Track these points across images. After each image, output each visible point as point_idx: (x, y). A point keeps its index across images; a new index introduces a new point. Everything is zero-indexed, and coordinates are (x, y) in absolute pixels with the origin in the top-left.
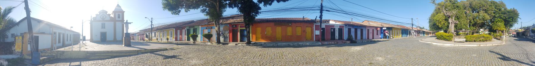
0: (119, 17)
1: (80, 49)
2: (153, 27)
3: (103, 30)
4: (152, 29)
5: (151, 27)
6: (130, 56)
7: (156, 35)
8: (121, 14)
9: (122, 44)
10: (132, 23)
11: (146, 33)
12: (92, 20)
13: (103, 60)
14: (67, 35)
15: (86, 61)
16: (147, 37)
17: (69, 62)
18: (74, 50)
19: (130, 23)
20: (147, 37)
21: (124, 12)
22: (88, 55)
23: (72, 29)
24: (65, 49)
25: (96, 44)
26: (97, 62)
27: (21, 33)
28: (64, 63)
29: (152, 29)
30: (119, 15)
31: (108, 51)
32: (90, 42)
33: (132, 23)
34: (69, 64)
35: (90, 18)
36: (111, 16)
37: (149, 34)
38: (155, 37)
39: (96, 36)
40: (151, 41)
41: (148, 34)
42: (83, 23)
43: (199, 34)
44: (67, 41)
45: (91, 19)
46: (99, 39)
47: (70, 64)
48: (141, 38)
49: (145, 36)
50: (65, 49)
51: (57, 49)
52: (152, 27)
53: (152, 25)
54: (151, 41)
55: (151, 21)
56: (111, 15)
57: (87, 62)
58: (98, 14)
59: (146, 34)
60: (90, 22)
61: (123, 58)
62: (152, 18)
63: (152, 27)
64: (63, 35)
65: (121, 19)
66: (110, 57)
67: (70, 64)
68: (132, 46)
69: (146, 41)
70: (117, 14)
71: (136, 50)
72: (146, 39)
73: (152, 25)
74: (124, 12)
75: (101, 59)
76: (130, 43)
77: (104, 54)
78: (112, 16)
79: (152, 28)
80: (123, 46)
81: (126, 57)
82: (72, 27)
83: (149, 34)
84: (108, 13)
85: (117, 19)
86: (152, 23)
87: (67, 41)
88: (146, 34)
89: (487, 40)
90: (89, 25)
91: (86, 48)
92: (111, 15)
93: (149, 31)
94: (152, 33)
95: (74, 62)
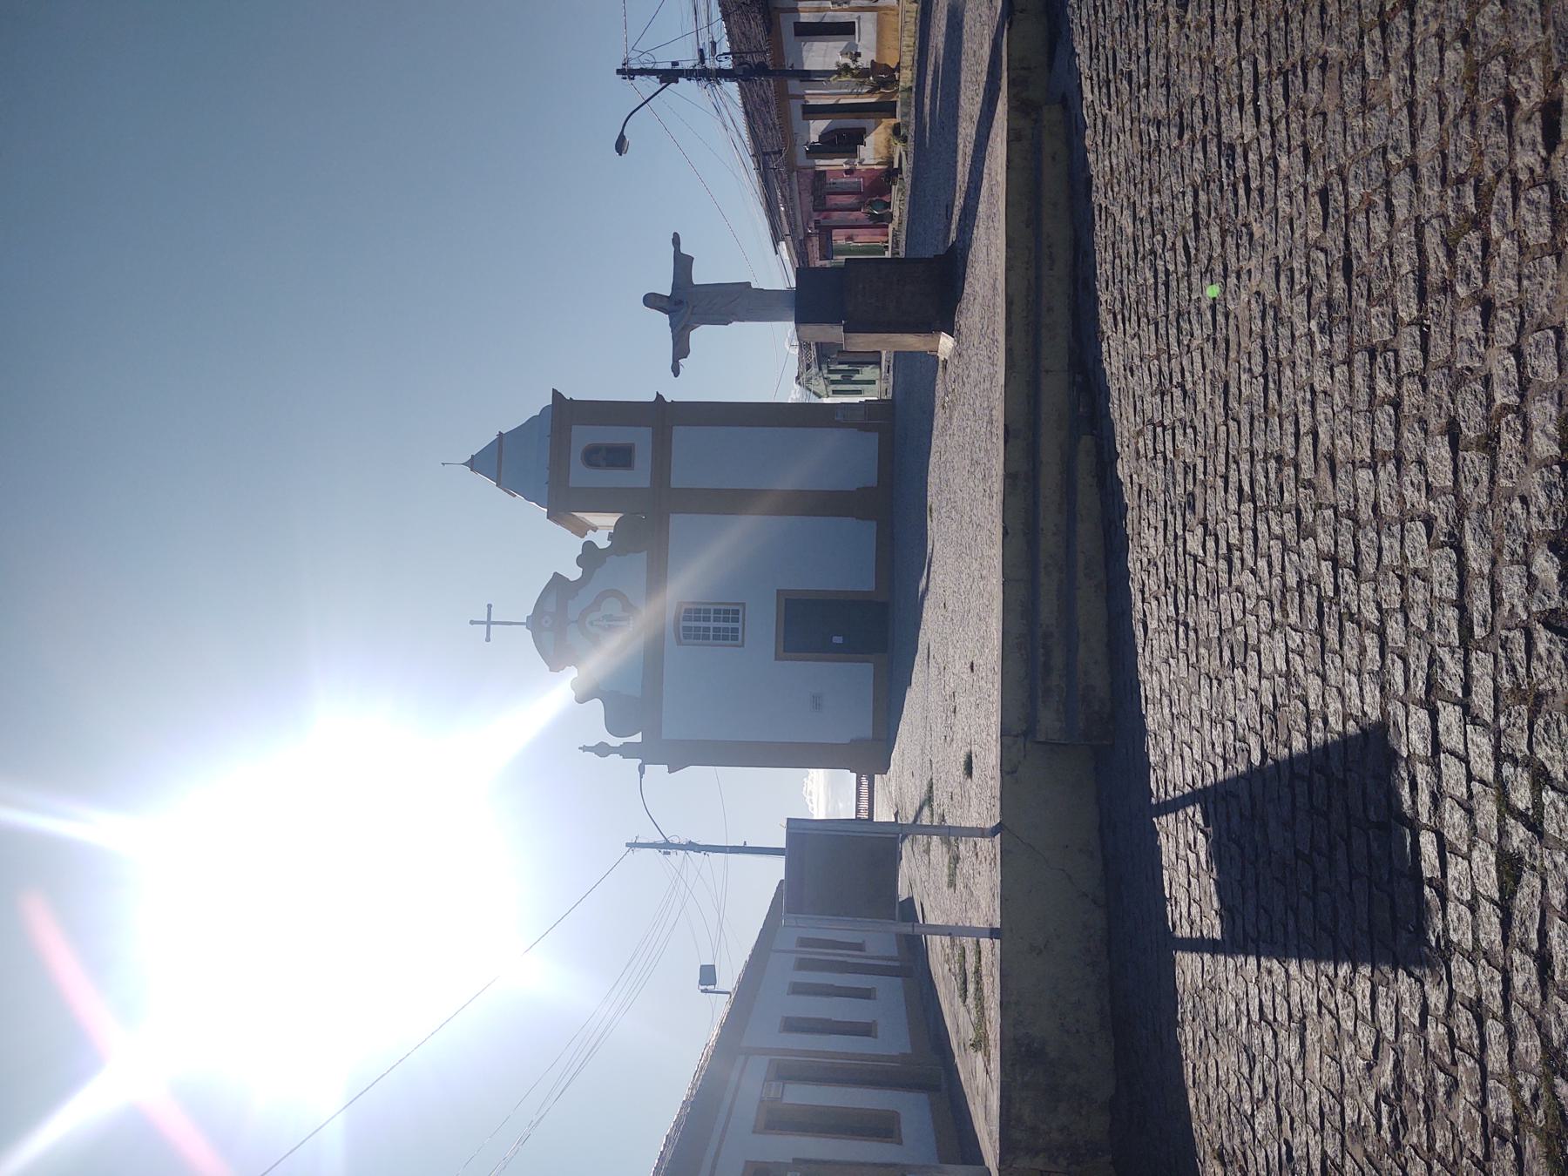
0: (620, 457)
1: (982, 833)
2: (727, 64)
3: (762, 624)
4: (761, 69)
5: (732, 88)
6: (1079, 183)
7: (830, 17)
8: (583, 436)
9: (930, 362)
10: (676, 240)
11: (802, 160)
12: (638, 738)
13: (1131, 515)
14: (793, 1025)
15: (1143, 731)
16: (858, 137)
17: (1168, 969)
18: (985, 908)
19: (683, 264)
20: (844, 142)
21: (556, 395)
22: (1049, 721)
23: (729, 978)
24: (979, 1043)
25: (913, 696)
26: (1152, 584)
27: (776, 659)
28: (1189, 1035)
29: (761, 69)
30: (599, 457)
31: (1010, 477)
32: (885, 768)
33: (676, 240)
34: (1189, 968)
35: (615, 758)
36: (602, 541)
37: (812, 112)
38: (847, 29)
39: (817, 702)
40: (906, 77)
41: (817, 127)
42: (666, 846)
43: (813, 167)
44: (866, 1030)
45: (626, 751)
46: (856, 677)
47: (1198, 945)
48: (860, 215)
49: (840, 163)
50: (979, 1043)
51: (976, 1157)
52: (722, 74)
53: (710, 64)
54: (906, 77)
55: (653, 83)
56: (591, 536)
57: (1154, 718)
58: (574, 573)
59: (815, 151)
60: (657, 771)
61: (1103, 257)
62: (627, 73)
63: (722, 74)
64: (803, 965)
65: (640, 438)
66: (1086, 442)
67: (1198, 945)
68: (953, 236)
69: (899, 148)
70: (581, 476)
71: (1013, 138)
72: (872, 151)
73: (702, 74)
74: (556, 395)
75: (1114, 543)
76: (921, 260)
77: (1050, 520)
78: (602, 525)
79: (744, 73)
80: (946, 343)
81: (1102, 233)
82: (708, 976)
83: (812, 112)
84: (574, 573)
85: (639, 476)
86: (689, 74)
87: (866, 1030)
88: (815, 151)
89: (1374, 45)
90: (695, 774)
91: (959, 771)
92: (591, 536)
93: (784, 114)
94: (807, 76)
95: (1157, 900)
